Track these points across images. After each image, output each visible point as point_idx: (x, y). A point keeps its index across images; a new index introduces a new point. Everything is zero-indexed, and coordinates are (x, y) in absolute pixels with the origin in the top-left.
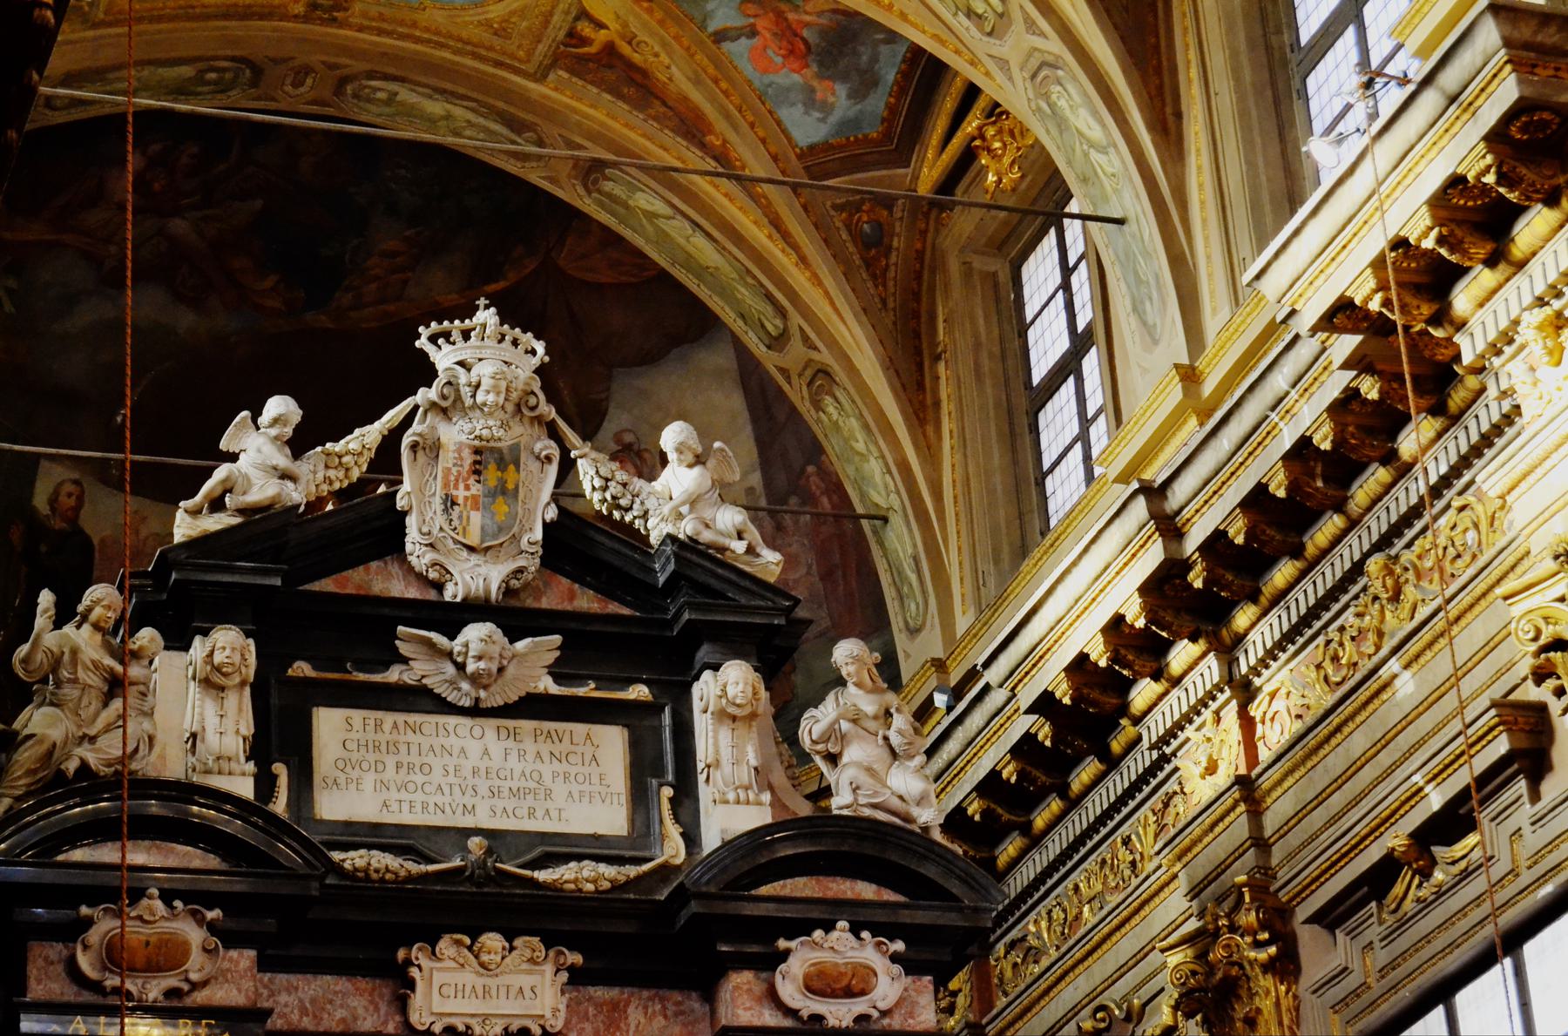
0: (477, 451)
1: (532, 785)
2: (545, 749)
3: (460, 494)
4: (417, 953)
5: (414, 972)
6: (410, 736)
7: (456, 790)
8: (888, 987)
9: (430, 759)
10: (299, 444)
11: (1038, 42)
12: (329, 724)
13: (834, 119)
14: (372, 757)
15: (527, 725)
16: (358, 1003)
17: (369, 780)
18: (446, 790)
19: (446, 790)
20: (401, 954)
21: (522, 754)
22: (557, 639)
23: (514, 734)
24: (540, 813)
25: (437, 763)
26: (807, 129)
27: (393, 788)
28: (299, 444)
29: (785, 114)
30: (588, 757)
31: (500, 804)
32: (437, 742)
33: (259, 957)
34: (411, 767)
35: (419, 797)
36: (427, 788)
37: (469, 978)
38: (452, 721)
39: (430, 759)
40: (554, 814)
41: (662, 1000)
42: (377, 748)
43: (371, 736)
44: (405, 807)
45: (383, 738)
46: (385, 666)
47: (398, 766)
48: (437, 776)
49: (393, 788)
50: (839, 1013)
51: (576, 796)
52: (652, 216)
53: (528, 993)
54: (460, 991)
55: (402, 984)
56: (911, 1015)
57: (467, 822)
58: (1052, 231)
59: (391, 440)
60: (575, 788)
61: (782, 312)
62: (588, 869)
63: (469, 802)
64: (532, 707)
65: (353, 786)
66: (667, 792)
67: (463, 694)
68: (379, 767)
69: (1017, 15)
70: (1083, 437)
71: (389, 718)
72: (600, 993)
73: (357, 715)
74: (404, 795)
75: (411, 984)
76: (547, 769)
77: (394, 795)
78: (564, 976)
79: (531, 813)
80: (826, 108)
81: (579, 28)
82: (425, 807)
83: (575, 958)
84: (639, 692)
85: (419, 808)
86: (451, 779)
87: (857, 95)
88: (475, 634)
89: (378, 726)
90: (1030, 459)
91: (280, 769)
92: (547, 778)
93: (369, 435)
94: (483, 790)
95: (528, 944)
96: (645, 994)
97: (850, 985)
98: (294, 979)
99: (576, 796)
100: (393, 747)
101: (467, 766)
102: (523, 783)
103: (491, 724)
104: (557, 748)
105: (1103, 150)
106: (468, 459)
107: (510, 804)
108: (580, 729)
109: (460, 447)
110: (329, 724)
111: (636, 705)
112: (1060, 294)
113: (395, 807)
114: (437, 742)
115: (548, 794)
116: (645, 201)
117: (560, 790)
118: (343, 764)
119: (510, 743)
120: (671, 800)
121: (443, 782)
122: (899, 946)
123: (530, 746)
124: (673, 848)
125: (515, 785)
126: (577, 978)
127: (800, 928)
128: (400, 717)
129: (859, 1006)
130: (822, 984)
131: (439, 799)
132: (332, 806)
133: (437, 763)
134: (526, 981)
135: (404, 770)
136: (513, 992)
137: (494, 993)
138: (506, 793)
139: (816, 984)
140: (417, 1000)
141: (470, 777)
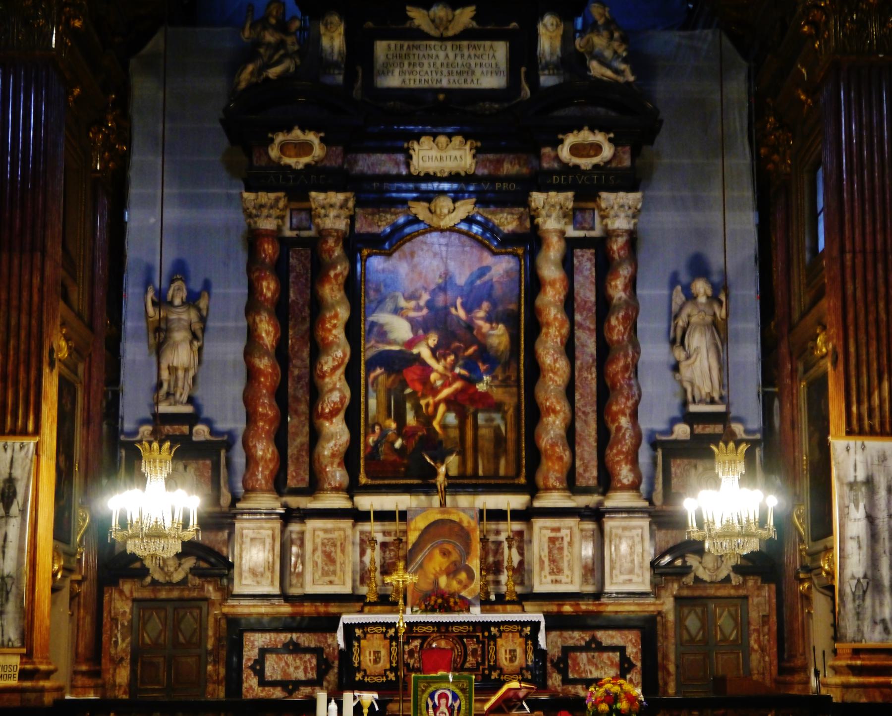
1: (466, 69)
2: (472, 53)
5: (411, 152)
6: (415, 51)
7: (434, 74)
8: (607, 151)
12: (381, 48)
14: (398, 61)
15: (465, 43)
17: (397, 71)
18: (430, 73)
19: (430, 73)
21: (462, 56)
23: (460, 48)
24: (469, 81)
25: (426, 62)
27: (407, 74)
30: (491, 56)
31: (452, 78)
32: (426, 53)
34: (414, 65)
35: (418, 77)
36: (421, 73)
37: (434, 153)
38: (432, 43)
40: (475, 81)
44: (412, 82)
47: (409, 64)
48: (426, 67)
49: (407, 74)
50: (586, 163)
51: (485, 73)
53: (458, 158)
54: (430, 158)
56: (620, 162)
60: (485, 70)
63: (439, 77)
64: (467, 35)
65: (390, 74)
66: (523, 70)
67: (433, 32)
68: (401, 65)
72: (491, 156)
74: (412, 77)
75: (410, 157)
77: (407, 77)
78: (473, 151)
79: (465, 81)
81: (377, 170)
82: (420, 81)
83: (479, 144)
84: (514, 25)
85: (417, 82)
86: (432, 68)
89: (402, 47)
90: (78, 449)
92: (473, 65)
96: (511, 156)
99: (485, 73)
100: (407, 56)
101: (438, 63)
102: (462, 69)
103: (449, 44)
104: (478, 53)
107: (456, 78)
110: (381, 48)
111: (514, 30)
113: (407, 82)
115: (473, 73)
117: (478, 71)
119: (458, 52)
120: (526, 73)
122: (612, 135)
124: (526, 92)
125: (459, 70)
126: (478, 152)
128: (411, 43)
129: (596, 160)
130: (576, 150)
131: (426, 77)
133: (426, 62)
134: (457, 153)
135: (411, 67)
136: (452, 159)
137: (445, 159)
138: (455, 73)
140: (415, 161)
141: (440, 67)
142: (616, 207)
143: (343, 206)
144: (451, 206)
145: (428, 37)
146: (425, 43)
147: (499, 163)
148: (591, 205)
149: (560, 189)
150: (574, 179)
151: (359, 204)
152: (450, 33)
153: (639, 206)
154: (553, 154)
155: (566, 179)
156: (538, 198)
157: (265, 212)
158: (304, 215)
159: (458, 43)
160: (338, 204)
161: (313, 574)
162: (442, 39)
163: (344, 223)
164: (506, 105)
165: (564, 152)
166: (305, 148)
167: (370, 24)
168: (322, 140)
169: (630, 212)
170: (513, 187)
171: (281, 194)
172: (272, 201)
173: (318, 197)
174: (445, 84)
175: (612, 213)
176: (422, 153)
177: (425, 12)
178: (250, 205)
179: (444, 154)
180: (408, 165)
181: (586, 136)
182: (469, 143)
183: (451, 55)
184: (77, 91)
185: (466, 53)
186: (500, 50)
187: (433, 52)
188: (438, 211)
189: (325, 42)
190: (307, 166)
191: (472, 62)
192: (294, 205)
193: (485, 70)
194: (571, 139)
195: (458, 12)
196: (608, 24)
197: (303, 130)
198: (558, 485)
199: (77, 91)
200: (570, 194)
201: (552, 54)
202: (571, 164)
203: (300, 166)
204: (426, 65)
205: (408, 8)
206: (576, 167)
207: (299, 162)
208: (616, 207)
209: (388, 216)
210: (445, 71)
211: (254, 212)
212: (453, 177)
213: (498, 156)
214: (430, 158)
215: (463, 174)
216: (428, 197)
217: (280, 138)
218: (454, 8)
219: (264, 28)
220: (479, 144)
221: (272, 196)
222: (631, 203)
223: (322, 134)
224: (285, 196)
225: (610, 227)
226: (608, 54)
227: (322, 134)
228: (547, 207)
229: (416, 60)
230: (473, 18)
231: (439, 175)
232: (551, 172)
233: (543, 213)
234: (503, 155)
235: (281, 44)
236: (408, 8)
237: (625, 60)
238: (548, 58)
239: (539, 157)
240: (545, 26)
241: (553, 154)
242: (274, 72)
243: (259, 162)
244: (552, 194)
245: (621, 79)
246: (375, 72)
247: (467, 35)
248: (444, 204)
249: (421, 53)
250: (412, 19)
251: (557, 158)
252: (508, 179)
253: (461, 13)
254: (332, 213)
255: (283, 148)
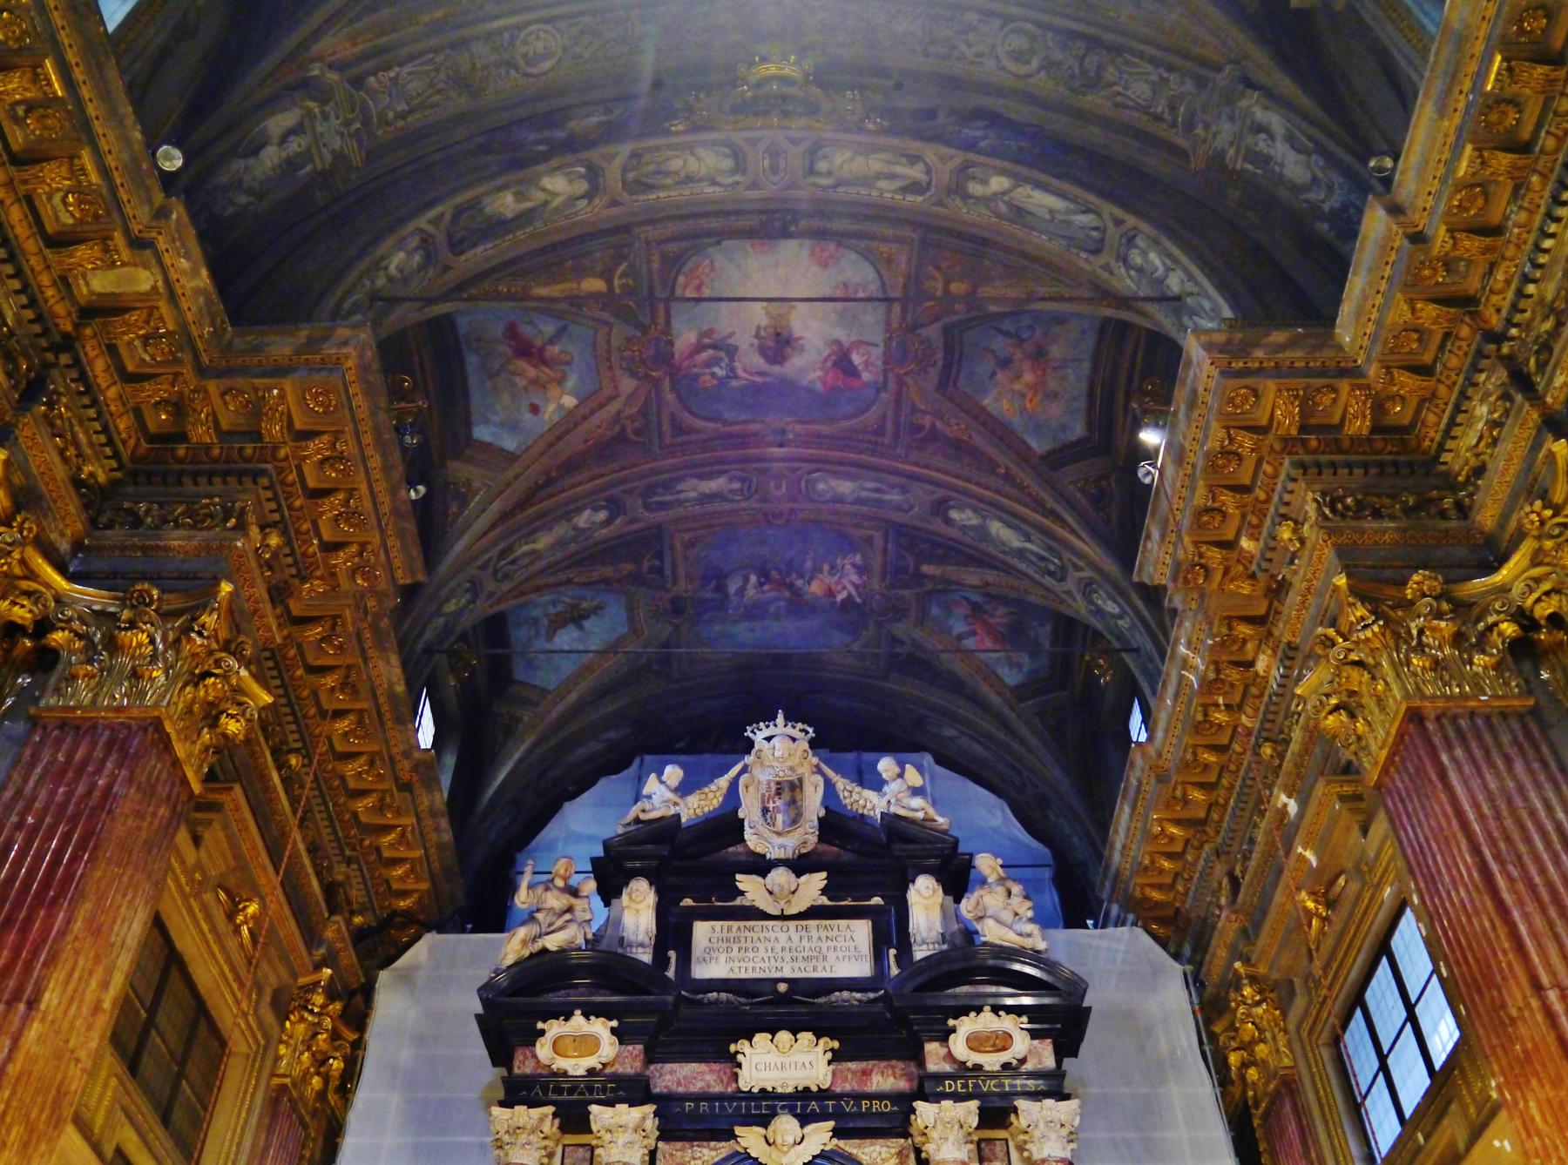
0: (778, 783)
2: (823, 934)
3: (771, 805)
4: (743, 1045)
8: (1021, 1044)
9: (758, 944)
10: (684, 789)
11: (1082, 574)
12: (702, 931)
13: (1025, 669)
14: (725, 945)
15: (812, 923)
16: (710, 1078)
17: (723, 957)
20: (733, 1048)
22: (824, 875)
25: (761, 947)
26: (1011, 677)
28: (684, 789)
29: (999, 671)
31: (796, 965)
32: (762, 936)
33: (647, 1051)
35: (751, 964)
37: (774, 1058)
38: (770, 923)
39: (758, 944)
41: (893, 1067)
42: (728, 940)
43: (725, 934)
45: (731, 935)
46: (734, 899)
48: (762, 953)
52: (952, 739)
54: (767, 1067)
55: (733, 1061)
57: (778, 975)
58: (1384, 960)
59: (734, 784)
60: (840, 954)
61: (1020, 773)
62: (845, 994)
63: (779, 964)
64: (813, 913)
66: (893, 952)
69: (1069, 564)
70: (1382, 1058)
71: (735, 924)
72: (853, 1065)
73: (718, 924)
75: (739, 1065)
76: (824, 946)
77: (737, 964)
78: (829, 1055)
80: (1019, 666)
83: (836, 1044)
84: (877, 900)
87: (1034, 655)
88: (780, 876)
89: (729, 929)
91: (672, 954)
93: (723, 782)
94: (787, 959)
95: (806, 1037)
97: (1002, 1042)
98: (675, 1066)
100: (737, 940)
101: (778, 947)
103: (792, 924)
104: (830, 934)
105: (1120, 617)
106: (774, 788)
108: (843, 923)
109: (769, 782)
110: (702, 931)
111: (878, 906)
112: (1413, 1000)
114: (762, 936)
115: (825, 958)
116: (949, 732)
117: (832, 956)
118: (709, 950)
120: (896, 956)
121: (765, 956)
123: (815, 934)
126: (837, 1057)
127: (962, 1011)
128: (742, 924)
129: (1005, 1057)
130: (975, 1043)
132: (701, 971)
133: (761, 947)
134: (805, 1058)
139: (974, 1044)
142: (1042, 1126)
143: (639, 1128)
144: (798, 1132)
145: (765, 916)
146: (760, 923)
147: (866, 1073)
148: (1002, 1134)
149: (958, 1097)
150: (976, 1086)
151: (666, 1134)
152: (793, 910)
153: (1077, 1122)
154: (943, 1051)
155: (965, 1086)
156: (925, 1112)
157: (523, 1138)
158: (581, 1152)
159: (804, 923)
160: (631, 1125)
161: (565, 299)
162: (783, 917)
163: (639, 1154)
164: (872, 995)
165: (958, 1045)
166: (588, 1044)
167: (688, 902)
168: (613, 1031)
169: (1064, 1132)
170: (887, 1107)
171: (550, 1109)
172: (534, 1122)
173: (600, 1115)
174: (788, 974)
175: (1037, 1134)
176: (755, 1059)
177: (760, 879)
178: (502, 1128)
179: (786, 1060)
180: (736, 1077)
181: (986, 1022)
182: (822, 1041)
183: (795, 937)
184: (253, 908)
185: (815, 934)
186: (861, 931)
187: (771, 935)
188: (779, 1141)
189: (628, 920)
190: (591, 1072)
191: (824, 946)
192: (570, 1139)
193: (840, 954)
194: (966, 1026)
195: (804, 878)
196: (1001, 880)
197: (586, 1016)
198: (466, 55)
199: (253, 908)
200: (974, 1105)
201: (930, 929)
202: (969, 1064)
203: (581, 1072)
204: (762, 949)
205: (738, 877)
206: (978, 1067)
207: (576, 1066)
208: (1042, 1126)
209: (706, 1151)
210: (787, 956)
211: (506, 1138)
212: (804, 1094)
213: (864, 1065)
214: (767, 1067)
215: (814, 1089)
216: (764, 1121)
217: (554, 1028)
218: (798, 875)
219: (547, 889)
220: (836, 1044)
221: (536, 1113)
222: (1063, 1118)
223: (614, 1023)
224: (555, 1115)
225: (1036, 1156)
226: (1007, 916)
227: (614, 1023)
228: (940, 1127)
229: (749, 945)
230: (824, 891)
231: (779, 1090)
232: (940, 1077)
233: (934, 1134)
234: (871, 1063)
235: (570, 910)
236: (738, 877)
237: (1031, 920)
238: (925, 934)
239: (918, 1057)
240: (919, 892)
241: (943, 1051)
242: (552, 942)
243: (523, 1066)
244: (947, 1104)
245: (1028, 943)
246: (694, 958)
247: (813, 913)
248: (788, 1126)
249: (755, 936)
250: (742, 893)
251: (950, 1056)
252: (880, 1096)
253: (808, 882)
254: (622, 1138)
255: (556, 1047)
